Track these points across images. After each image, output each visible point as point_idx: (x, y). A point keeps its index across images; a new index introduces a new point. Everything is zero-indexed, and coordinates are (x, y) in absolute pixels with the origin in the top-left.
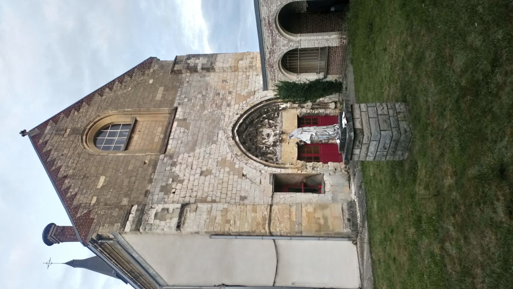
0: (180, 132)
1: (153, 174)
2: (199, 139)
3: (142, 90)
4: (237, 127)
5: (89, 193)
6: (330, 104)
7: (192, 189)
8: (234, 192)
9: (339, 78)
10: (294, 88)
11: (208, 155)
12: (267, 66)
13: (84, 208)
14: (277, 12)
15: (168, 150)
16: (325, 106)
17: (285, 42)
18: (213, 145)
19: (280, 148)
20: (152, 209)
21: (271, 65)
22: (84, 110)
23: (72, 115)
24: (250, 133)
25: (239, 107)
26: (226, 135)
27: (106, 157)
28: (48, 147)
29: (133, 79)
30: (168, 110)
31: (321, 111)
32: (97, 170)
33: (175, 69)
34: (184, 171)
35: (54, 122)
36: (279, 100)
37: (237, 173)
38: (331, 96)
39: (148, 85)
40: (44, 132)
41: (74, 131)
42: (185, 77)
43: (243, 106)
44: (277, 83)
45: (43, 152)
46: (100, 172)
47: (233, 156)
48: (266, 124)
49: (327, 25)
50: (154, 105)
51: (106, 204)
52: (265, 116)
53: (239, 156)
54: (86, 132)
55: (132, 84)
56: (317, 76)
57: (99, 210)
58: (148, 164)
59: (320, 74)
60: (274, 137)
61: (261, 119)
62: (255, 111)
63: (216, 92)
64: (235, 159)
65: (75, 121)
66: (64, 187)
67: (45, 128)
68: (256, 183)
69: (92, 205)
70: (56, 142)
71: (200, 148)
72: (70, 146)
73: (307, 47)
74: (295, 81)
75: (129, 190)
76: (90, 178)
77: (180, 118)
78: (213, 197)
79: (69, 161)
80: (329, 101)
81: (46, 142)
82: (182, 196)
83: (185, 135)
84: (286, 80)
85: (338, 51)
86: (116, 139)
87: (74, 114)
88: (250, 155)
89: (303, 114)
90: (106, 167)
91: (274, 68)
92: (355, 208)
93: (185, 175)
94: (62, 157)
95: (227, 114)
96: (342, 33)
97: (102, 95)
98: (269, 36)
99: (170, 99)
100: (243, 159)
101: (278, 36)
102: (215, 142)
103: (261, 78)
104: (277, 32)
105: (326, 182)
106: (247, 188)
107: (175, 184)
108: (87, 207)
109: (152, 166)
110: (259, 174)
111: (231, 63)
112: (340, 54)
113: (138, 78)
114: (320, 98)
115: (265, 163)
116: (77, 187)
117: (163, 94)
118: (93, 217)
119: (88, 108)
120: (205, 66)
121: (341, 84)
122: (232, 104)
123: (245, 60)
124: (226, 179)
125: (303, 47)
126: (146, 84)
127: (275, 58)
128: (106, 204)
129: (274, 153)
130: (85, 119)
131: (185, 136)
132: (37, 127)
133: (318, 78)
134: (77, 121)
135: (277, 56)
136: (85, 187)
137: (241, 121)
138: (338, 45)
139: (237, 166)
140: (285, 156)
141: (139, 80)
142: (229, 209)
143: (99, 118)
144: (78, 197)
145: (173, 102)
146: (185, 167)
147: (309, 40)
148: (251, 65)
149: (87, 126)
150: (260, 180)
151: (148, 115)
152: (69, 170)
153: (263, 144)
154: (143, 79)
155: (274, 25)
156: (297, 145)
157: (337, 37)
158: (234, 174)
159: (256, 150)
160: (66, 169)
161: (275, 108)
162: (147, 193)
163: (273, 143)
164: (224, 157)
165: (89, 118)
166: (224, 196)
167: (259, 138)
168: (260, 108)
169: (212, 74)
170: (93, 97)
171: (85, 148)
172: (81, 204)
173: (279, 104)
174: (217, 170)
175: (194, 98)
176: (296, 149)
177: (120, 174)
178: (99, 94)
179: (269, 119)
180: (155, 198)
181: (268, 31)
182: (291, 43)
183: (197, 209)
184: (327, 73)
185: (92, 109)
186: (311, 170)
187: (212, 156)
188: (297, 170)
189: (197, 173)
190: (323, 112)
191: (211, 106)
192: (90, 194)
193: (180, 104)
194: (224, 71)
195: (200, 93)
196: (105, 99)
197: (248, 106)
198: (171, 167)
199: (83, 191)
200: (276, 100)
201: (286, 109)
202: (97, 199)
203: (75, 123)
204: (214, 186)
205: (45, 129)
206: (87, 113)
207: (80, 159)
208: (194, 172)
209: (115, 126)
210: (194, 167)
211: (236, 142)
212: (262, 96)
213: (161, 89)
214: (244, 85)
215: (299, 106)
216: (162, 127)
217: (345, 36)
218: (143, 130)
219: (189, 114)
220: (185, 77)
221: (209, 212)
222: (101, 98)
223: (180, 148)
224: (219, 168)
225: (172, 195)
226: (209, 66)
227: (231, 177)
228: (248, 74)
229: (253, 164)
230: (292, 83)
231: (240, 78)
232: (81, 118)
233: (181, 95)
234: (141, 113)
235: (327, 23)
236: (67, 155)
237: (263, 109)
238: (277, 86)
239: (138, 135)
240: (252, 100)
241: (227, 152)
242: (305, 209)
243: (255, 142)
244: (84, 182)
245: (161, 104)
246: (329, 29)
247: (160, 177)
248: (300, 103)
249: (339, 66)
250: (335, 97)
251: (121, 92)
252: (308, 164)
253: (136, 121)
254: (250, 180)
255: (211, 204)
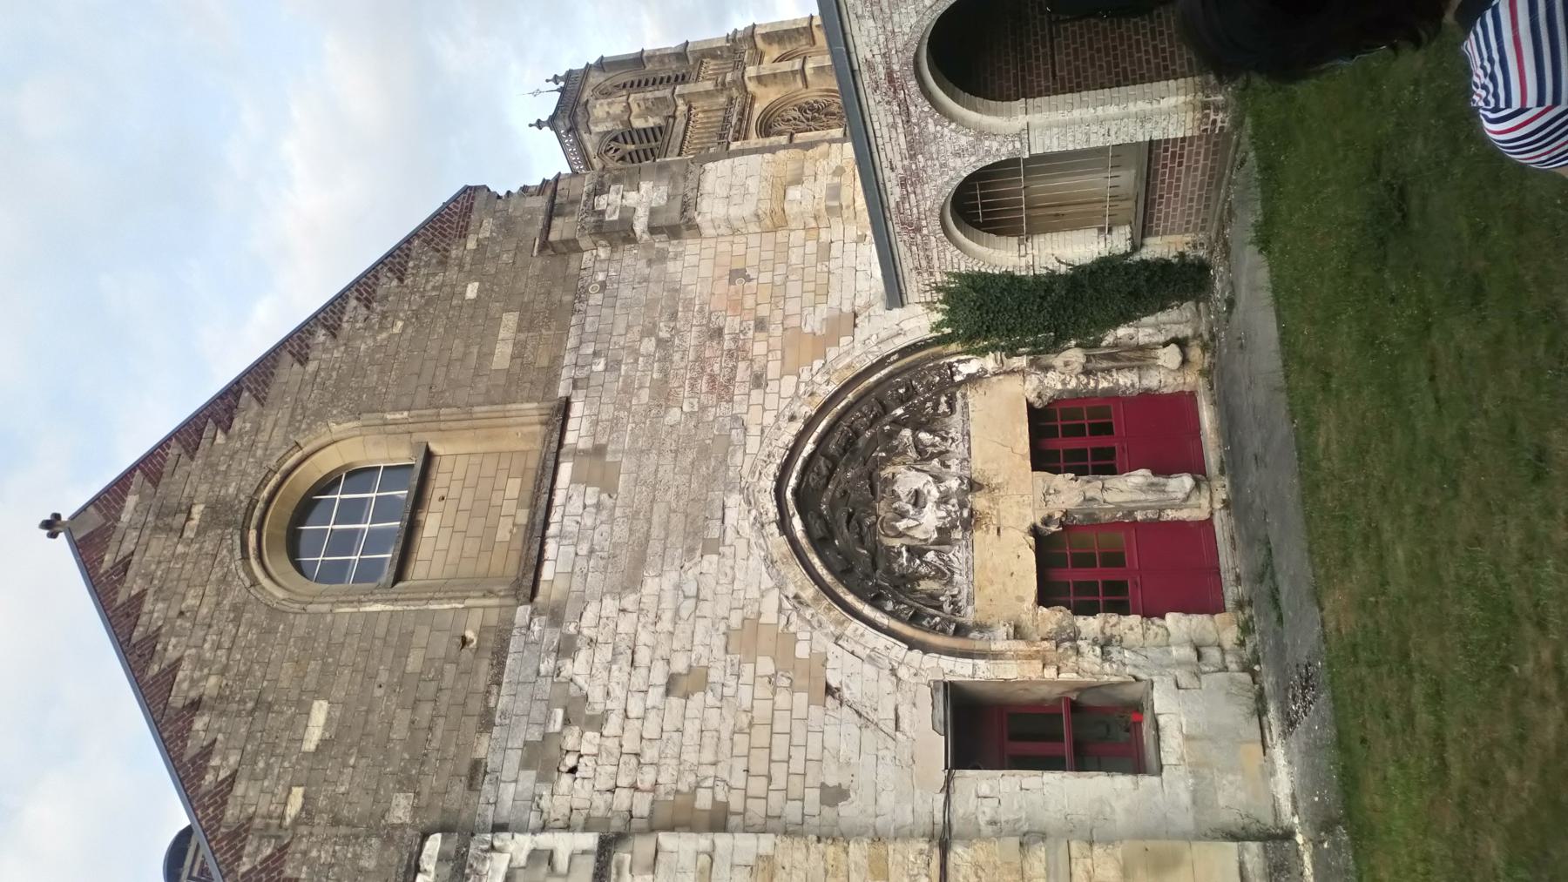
0: (585, 507)
1: (494, 689)
2: (655, 532)
3: (441, 330)
4: (794, 475)
5: (276, 771)
6: (1161, 352)
7: (637, 755)
8: (797, 765)
9: (1195, 247)
10: (1010, 293)
11: (691, 602)
12: (895, 227)
13: (261, 838)
14: (919, 35)
15: (543, 587)
16: (1140, 356)
17: (963, 141)
18: (706, 557)
19: (966, 555)
20: (494, 855)
21: (910, 225)
22: (248, 425)
23: (208, 446)
24: (845, 492)
25: (797, 387)
26: (754, 512)
27: (329, 618)
28: (134, 585)
29: (406, 286)
30: (537, 409)
31: (1126, 380)
32: (301, 674)
33: (553, 236)
34: (605, 674)
35: (150, 480)
36: (953, 347)
37: (805, 682)
38: (1162, 316)
39: (461, 307)
40: (118, 519)
41: (217, 513)
42: (591, 264)
43: (813, 382)
44: (939, 280)
45: (119, 602)
46: (311, 682)
47: (786, 605)
48: (906, 447)
49: (1138, 41)
50: (488, 391)
51: (336, 822)
52: (899, 411)
53: (808, 605)
54: (257, 513)
55: (406, 307)
56: (1102, 244)
57: (314, 844)
58: (475, 642)
59: (1115, 233)
60: (938, 508)
61: (888, 427)
62: (860, 399)
63: (707, 325)
64: (794, 618)
65: (218, 473)
66: (192, 748)
67: (118, 504)
68: (881, 725)
69: (288, 821)
70: (159, 562)
71: (660, 575)
72: (205, 578)
73: (1055, 149)
74: (1010, 269)
75: (413, 760)
76: (276, 707)
77: (581, 446)
78: (717, 789)
79: (205, 640)
80: (1155, 339)
81: (124, 565)
82: (604, 787)
83: (604, 519)
84: (976, 269)
85: (1190, 152)
86: (364, 530)
87: (212, 443)
88: (850, 599)
89: (1049, 393)
90: (330, 660)
91: (925, 231)
92: (1295, 873)
93: (608, 693)
94: (179, 622)
95: (753, 418)
96: (1207, 83)
97: (303, 360)
98: (894, 126)
99: (544, 361)
100: (824, 618)
101: (930, 120)
102: (712, 546)
103: (870, 251)
104: (926, 109)
105: (1162, 720)
106: (847, 749)
107: (576, 734)
108: (273, 831)
109: (489, 655)
110: (887, 684)
111: (759, 200)
112: (1197, 161)
113: (426, 278)
114: (1116, 325)
115: (907, 631)
116: (235, 748)
117: (515, 345)
118: (295, 876)
119: (260, 414)
120: (661, 221)
121: (1203, 268)
122: (769, 377)
123: (808, 183)
124: (762, 710)
125: (1037, 150)
126: (455, 302)
127: (925, 199)
128: (336, 822)
129: (944, 574)
130: (251, 460)
131: (602, 523)
132: (92, 502)
133: (1105, 253)
134: (226, 472)
135: (934, 193)
136: (264, 746)
137: (809, 447)
138: (1189, 134)
139: (802, 651)
140: (989, 591)
141: (429, 287)
142: (779, 859)
143: (298, 455)
144: (239, 789)
145: (551, 376)
146: (609, 657)
147: (1066, 125)
148: (836, 204)
149: (258, 490)
150: (896, 710)
151: (470, 434)
152: (207, 677)
153: (900, 535)
154: (443, 285)
155: (913, 84)
156: (1031, 540)
157: (1185, 103)
158: (792, 689)
159: (875, 567)
160: (197, 674)
161: (938, 378)
162: (476, 773)
163: (935, 535)
164: (750, 611)
165: (265, 455)
166: (757, 786)
167: (882, 507)
168: (879, 383)
169: (691, 246)
170: (274, 367)
171: (255, 583)
172: (250, 819)
173: (954, 359)
174: (728, 671)
175: (628, 355)
176: (1030, 558)
177: (378, 692)
178: (293, 355)
179: (917, 427)
180: (505, 797)
181: (888, 107)
182: (987, 143)
183: (660, 856)
184: (1144, 230)
185: (271, 419)
186: (1099, 661)
187: (705, 608)
188: (1038, 664)
189: (655, 686)
190: (1133, 385)
191: (692, 386)
192: (279, 777)
193: (579, 384)
194: (735, 232)
195: (650, 331)
196: (316, 374)
197: (833, 378)
198: (557, 660)
199: (256, 763)
200: (939, 349)
201: (981, 377)
202: (305, 796)
203: (218, 478)
204: (719, 739)
205: (122, 508)
206: (256, 435)
207: (241, 630)
208: (641, 681)
209: (358, 476)
210: (643, 656)
211: (793, 542)
212: (883, 335)
213: (510, 320)
214: (811, 286)
215: (1031, 363)
216: (523, 476)
217: (1220, 98)
218: (454, 493)
219: (612, 428)
220: (591, 264)
221: (701, 872)
222: (302, 369)
223: (586, 575)
224: (736, 661)
225: (566, 779)
226: (674, 216)
227: (782, 699)
228: (824, 236)
229: (862, 641)
230: (1001, 276)
231: (795, 257)
232: (237, 457)
233: (581, 343)
234: (442, 426)
235: (1137, 33)
236: (195, 611)
237: (891, 386)
238: (938, 290)
239: (439, 516)
240: (848, 353)
241: (763, 587)
242: (1085, 865)
243: (869, 527)
244: (258, 726)
245: (508, 389)
246: (1148, 62)
247: (521, 705)
248: (1034, 353)
249: (1194, 204)
250: (1177, 319)
251: (370, 342)
252: (1081, 621)
253: (429, 456)
254: (857, 712)
255: (710, 835)
